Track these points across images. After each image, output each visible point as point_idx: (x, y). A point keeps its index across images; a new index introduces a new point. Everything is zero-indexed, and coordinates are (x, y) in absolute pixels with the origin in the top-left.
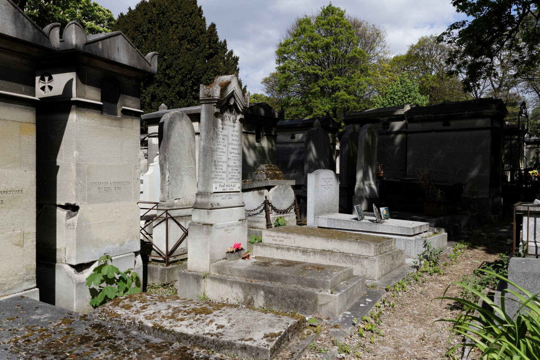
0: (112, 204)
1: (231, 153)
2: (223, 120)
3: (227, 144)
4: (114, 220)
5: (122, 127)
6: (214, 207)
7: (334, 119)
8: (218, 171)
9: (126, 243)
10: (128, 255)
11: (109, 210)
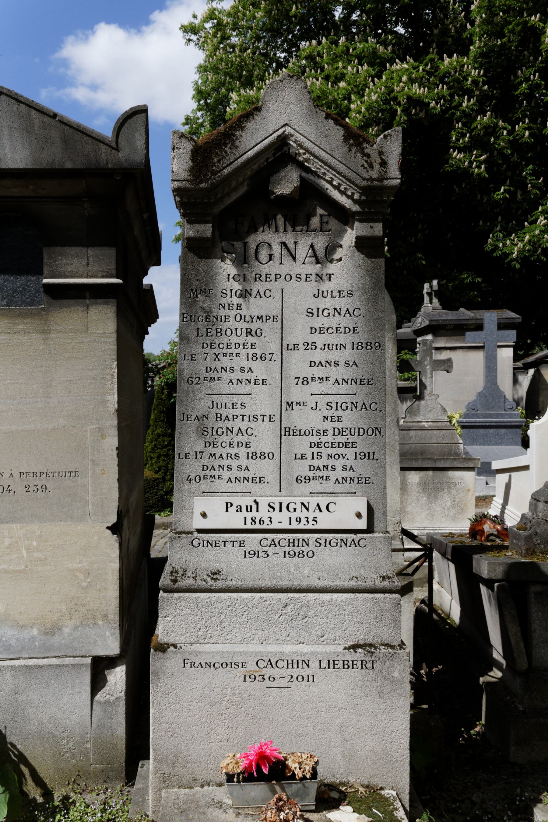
0: (16, 526)
1: (305, 381)
2: (242, 261)
3: (273, 346)
6: (187, 582)
7: (382, 136)
8: (218, 451)
9: (66, 630)
10: (67, 661)
11: (7, 541)
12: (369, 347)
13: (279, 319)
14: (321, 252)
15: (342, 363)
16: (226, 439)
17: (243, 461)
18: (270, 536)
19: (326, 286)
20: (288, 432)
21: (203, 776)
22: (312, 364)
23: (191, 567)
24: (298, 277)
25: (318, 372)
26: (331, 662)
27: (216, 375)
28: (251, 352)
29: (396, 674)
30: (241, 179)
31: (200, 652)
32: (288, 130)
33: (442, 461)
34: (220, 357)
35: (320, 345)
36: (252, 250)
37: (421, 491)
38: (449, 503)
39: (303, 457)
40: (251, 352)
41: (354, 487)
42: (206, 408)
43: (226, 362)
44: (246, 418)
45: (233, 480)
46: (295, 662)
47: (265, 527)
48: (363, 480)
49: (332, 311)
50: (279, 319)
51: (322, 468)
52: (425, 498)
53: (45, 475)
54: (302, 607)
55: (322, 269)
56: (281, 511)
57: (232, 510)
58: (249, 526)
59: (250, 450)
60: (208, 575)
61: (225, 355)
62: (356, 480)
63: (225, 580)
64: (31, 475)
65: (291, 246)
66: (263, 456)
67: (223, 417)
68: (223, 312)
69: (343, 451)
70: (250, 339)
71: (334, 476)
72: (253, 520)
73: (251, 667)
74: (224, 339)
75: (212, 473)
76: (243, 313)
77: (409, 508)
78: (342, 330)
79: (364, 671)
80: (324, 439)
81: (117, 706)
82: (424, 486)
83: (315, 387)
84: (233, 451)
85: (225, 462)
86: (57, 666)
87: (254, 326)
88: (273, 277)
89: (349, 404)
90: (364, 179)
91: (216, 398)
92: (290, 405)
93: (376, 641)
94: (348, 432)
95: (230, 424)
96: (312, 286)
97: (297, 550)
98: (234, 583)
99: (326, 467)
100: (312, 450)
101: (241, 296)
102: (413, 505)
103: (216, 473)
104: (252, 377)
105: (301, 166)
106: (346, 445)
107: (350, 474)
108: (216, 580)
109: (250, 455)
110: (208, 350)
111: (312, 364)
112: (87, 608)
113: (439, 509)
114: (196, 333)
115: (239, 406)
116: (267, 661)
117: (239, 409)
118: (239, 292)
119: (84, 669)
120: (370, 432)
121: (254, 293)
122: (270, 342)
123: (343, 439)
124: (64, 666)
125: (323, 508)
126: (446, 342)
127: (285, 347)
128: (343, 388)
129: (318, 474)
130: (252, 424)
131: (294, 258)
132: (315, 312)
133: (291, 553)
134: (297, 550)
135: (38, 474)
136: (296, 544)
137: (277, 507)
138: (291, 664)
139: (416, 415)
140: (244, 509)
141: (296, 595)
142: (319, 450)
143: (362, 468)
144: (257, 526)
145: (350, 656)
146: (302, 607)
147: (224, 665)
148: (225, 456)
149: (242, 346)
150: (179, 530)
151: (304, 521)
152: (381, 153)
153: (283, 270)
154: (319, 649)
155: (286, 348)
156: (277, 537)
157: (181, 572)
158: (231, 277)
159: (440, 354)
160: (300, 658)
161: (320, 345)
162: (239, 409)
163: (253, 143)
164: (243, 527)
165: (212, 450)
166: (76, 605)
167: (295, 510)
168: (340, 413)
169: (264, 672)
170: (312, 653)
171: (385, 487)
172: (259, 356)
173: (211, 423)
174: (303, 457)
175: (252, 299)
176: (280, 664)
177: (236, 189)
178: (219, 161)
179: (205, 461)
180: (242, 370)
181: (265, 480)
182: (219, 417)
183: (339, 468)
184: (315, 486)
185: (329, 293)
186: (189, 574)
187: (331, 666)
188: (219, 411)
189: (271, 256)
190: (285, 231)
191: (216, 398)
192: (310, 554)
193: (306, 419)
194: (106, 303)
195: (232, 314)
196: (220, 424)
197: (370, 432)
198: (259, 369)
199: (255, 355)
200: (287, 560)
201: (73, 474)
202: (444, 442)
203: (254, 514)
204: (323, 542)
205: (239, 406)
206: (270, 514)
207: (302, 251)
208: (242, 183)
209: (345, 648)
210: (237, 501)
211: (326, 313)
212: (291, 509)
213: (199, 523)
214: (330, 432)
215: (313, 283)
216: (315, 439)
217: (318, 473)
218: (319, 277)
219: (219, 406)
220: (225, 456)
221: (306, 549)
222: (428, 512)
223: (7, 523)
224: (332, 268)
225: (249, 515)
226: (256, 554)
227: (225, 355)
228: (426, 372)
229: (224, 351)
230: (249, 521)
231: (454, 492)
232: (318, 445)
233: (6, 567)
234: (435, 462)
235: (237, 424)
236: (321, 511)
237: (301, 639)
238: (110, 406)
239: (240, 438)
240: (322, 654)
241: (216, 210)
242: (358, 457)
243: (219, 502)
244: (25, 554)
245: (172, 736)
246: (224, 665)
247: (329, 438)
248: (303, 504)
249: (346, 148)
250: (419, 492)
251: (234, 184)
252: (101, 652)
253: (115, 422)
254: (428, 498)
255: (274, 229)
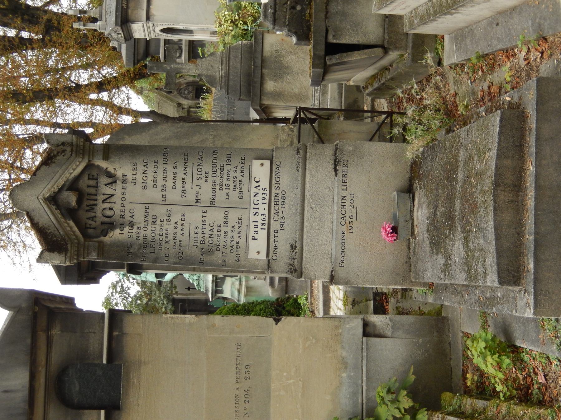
0: (273, 386)
1: (184, 192)
4: (301, 383)
5: (140, 362)
8: (222, 243)
9: (344, 354)
11: (282, 393)
12: (166, 155)
13: (147, 205)
14: (110, 180)
15: (174, 170)
16: (215, 238)
17: (229, 229)
18: (272, 215)
19: (130, 177)
20: (213, 202)
21: (406, 259)
22: (174, 188)
23: (288, 261)
24: (124, 193)
25: (179, 184)
26: (343, 184)
27: (178, 243)
28: (165, 222)
29: (351, 149)
30: (66, 225)
31: (336, 257)
32: (41, 197)
33: (256, 61)
34: (167, 240)
35: (164, 183)
36: (106, 220)
37: (281, 80)
38: (293, 56)
39: (228, 195)
40: (165, 222)
41: (246, 166)
42: (197, 250)
43: (171, 237)
44: (204, 226)
45: (239, 235)
46: (343, 204)
47: (267, 218)
48: (243, 161)
49: (144, 175)
50: (147, 205)
51: (234, 184)
52: (288, 77)
53: (238, 366)
54: (313, 199)
55: (119, 180)
56: (258, 209)
57: (256, 236)
58: (266, 227)
59: (223, 225)
60: (293, 251)
61: (166, 237)
62: (242, 165)
63: (296, 241)
64: (238, 375)
65: (105, 197)
66: (226, 218)
67: (203, 239)
68: (142, 238)
69: (225, 172)
70: (158, 222)
71: (239, 178)
72: (263, 224)
73: (344, 229)
74: (157, 237)
75: (235, 247)
76: (142, 226)
77: (296, 91)
78: (155, 169)
79: (349, 165)
80: (218, 182)
81: (395, 321)
82: (277, 77)
83: (188, 186)
84: (223, 235)
85: (229, 239)
86: (367, 360)
87: (150, 220)
88: (123, 208)
89: (199, 167)
90: (71, 155)
91: (192, 243)
92: (197, 201)
93: (333, 158)
94: (214, 169)
95: (207, 236)
96: (129, 186)
97: (281, 200)
98: (297, 237)
99: (234, 182)
100: (224, 189)
101: (132, 227)
102: (293, 87)
103: (235, 245)
104: (180, 222)
105: (60, 190)
106: (222, 170)
107: (239, 169)
108: (296, 247)
109: (225, 225)
110: (163, 247)
111: (174, 188)
112: (330, 340)
113: (298, 66)
114: (153, 254)
115: (196, 230)
116: (341, 220)
117: (199, 230)
118: (130, 228)
119: (370, 342)
120: (215, 156)
121: (131, 219)
122: (161, 211)
123: (219, 171)
124: (367, 356)
125: (257, 184)
126: (141, 8)
127: (163, 203)
128: (189, 170)
129: (238, 187)
130: (207, 223)
131: (112, 195)
132: (144, 185)
133: (282, 203)
134: (281, 200)
135: (238, 371)
136: (277, 201)
137: (256, 211)
138: (343, 207)
139: (215, 79)
140: (256, 230)
141: (306, 202)
142: (224, 185)
143: (235, 161)
144: (266, 222)
145: (340, 173)
146: (313, 199)
147: (343, 244)
148: (226, 239)
149: (162, 227)
150: (267, 267)
151: (264, 196)
152: (58, 145)
153: (119, 202)
154: (336, 190)
155: (164, 202)
156: (273, 211)
157: (290, 267)
158: (121, 232)
159: (154, 15)
160: (340, 201)
161: (164, 183)
162: (199, 230)
163: (47, 217)
164: (266, 231)
165: (221, 247)
166: (327, 347)
167: (258, 200)
168: (203, 173)
169: (347, 222)
170: (338, 194)
171: (247, 149)
172: (168, 218)
173: (205, 247)
174: (228, 195)
175: (135, 221)
176: (343, 212)
177: (71, 228)
178: (55, 237)
179: (228, 251)
180: (176, 228)
181: (240, 217)
182: (203, 242)
183: (235, 175)
184: (245, 189)
185: (134, 176)
186: (292, 262)
187: (345, 184)
188: (199, 242)
189: (110, 209)
190: (96, 200)
191: (192, 243)
192: (284, 193)
193: (206, 194)
194: (122, 321)
195: (142, 232)
196: (207, 241)
197: (215, 156)
198: (176, 218)
199: (167, 220)
200: (286, 206)
201: (239, 347)
202: (240, 57)
203: (259, 224)
204: (277, 186)
205: (196, 230)
206: (260, 214)
207: (108, 191)
208: (68, 224)
209: (336, 176)
210: (251, 234)
211: (145, 178)
212: (257, 203)
213: (263, 256)
214: (214, 178)
215: (127, 185)
216: (218, 187)
217: (238, 186)
218: (124, 181)
219: (196, 242)
220: (226, 239)
221: (281, 195)
222: (300, 75)
223: (270, 393)
224: (119, 173)
225: (260, 227)
226: (282, 224)
227: (166, 237)
228: (177, 68)
229: (164, 238)
230: (263, 227)
231: (284, 52)
232: (221, 186)
233: (300, 394)
234: (257, 67)
235: (207, 232)
236: (259, 186)
237: (331, 200)
238: (193, 320)
239: (215, 230)
240: (338, 189)
241: (82, 239)
242: (229, 163)
243: (252, 243)
244: (292, 381)
245: (382, 275)
246: (343, 244)
247: (218, 179)
248: (254, 196)
249: (53, 165)
250: (282, 82)
251: (68, 229)
252: (360, 331)
253: (204, 317)
254: (288, 74)
255: (94, 206)
